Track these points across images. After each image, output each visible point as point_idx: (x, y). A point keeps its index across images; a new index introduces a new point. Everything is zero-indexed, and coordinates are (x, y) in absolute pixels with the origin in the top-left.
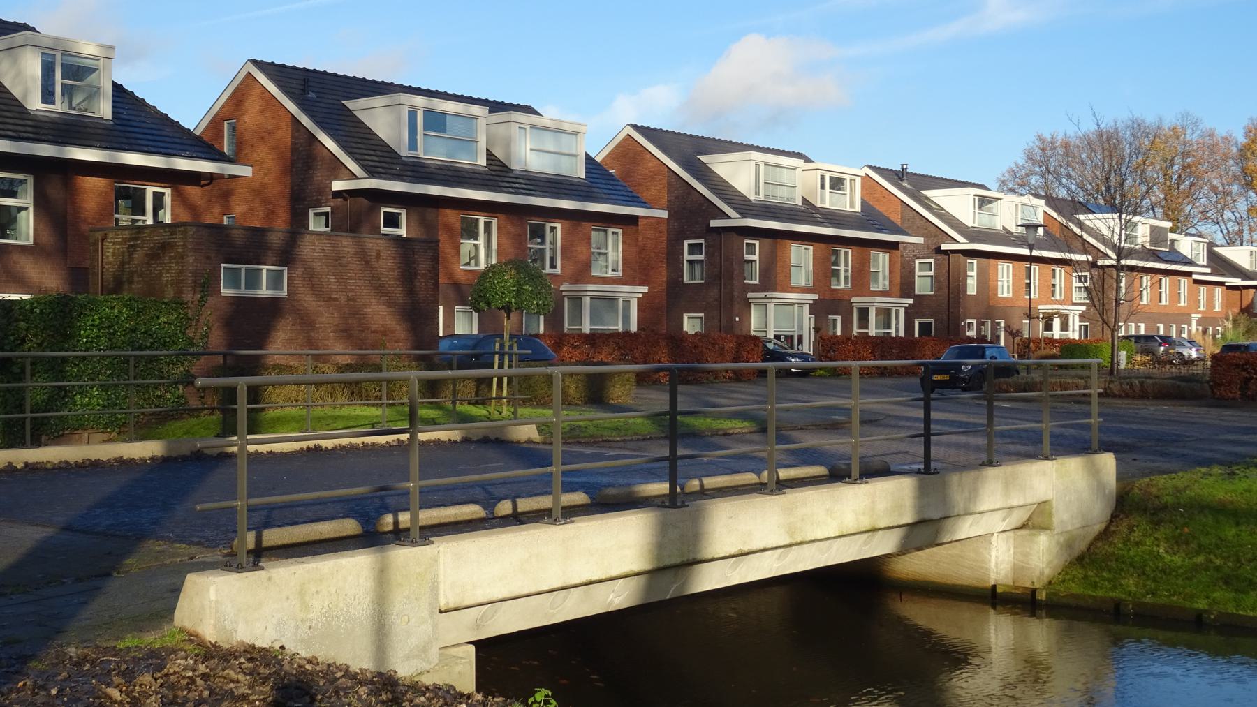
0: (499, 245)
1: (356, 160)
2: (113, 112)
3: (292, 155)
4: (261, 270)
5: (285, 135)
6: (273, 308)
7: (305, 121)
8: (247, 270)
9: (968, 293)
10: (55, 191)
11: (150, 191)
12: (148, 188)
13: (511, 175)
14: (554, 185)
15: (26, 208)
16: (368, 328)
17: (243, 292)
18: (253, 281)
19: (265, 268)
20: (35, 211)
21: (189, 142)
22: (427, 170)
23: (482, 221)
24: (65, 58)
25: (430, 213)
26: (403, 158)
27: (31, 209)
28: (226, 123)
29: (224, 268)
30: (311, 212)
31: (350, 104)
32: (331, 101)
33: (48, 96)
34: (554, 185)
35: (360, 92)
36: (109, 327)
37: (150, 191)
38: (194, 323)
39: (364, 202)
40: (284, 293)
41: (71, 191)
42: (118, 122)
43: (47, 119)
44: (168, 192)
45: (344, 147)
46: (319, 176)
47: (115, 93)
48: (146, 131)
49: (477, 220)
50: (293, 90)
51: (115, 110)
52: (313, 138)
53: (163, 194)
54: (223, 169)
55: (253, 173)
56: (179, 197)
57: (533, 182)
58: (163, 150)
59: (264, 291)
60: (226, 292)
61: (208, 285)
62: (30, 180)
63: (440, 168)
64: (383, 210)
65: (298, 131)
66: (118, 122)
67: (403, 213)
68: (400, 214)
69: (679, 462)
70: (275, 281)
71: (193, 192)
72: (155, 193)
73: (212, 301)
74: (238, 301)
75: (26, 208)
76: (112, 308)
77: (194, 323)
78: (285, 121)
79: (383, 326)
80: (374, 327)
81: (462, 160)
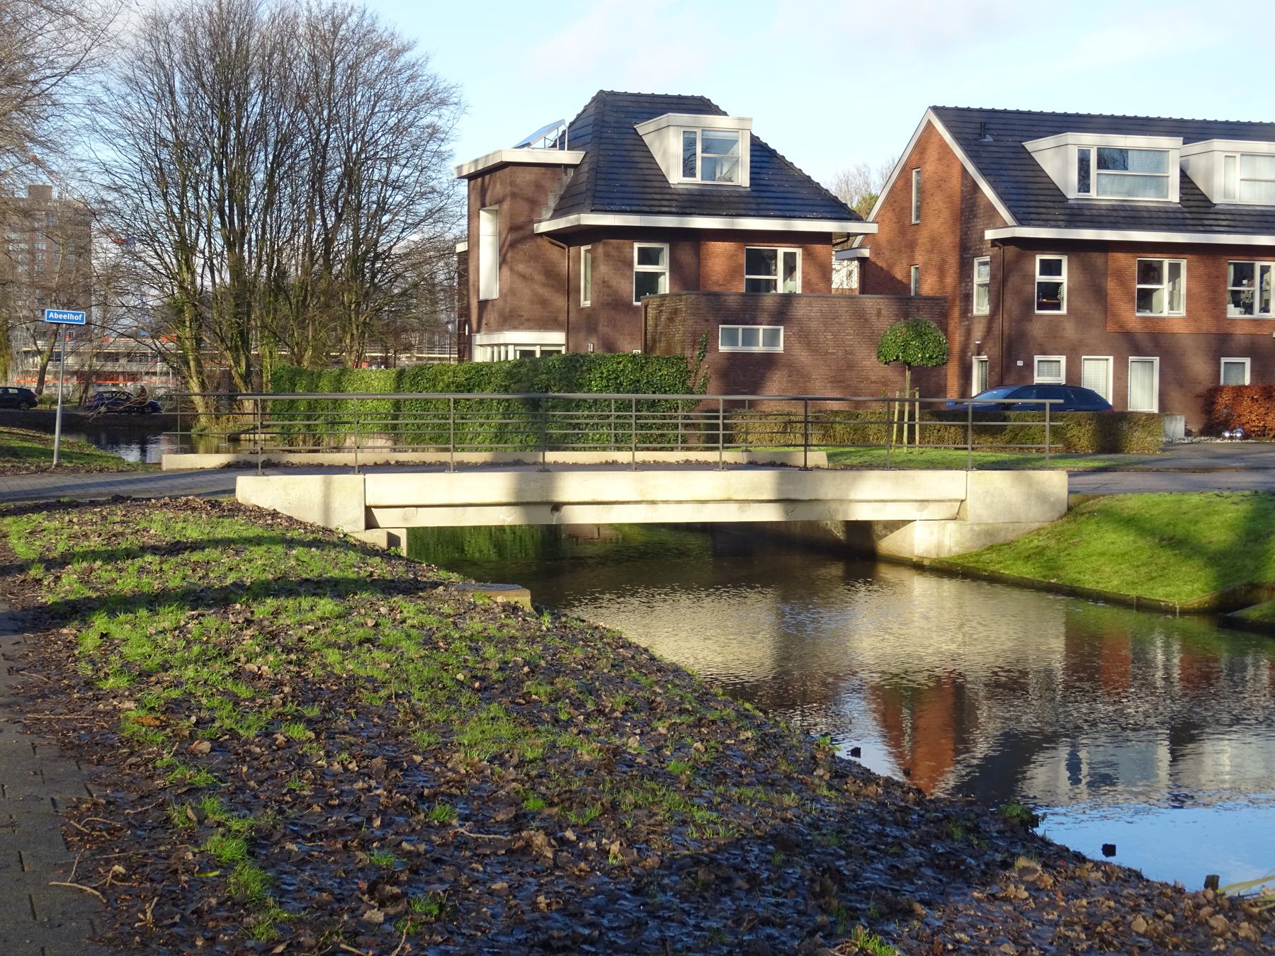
0: (1188, 290)
1: (1009, 208)
2: (751, 179)
3: (962, 204)
4: (758, 329)
5: (955, 182)
6: (768, 361)
7: (971, 169)
9: (1064, 383)
10: (686, 256)
11: (781, 251)
13: (1212, 210)
14: (1209, 228)
15: (664, 274)
16: (867, 379)
17: (740, 348)
18: (750, 338)
19: (761, 328)
20: (670, 275)
21: (821, 203)
22: (1095, 212)
23: (1166, 263)
25: (1098, 258)
26: (1070, 202)
27: (667, 274)
28: (914, 172)
30: (976, 262)
31: (1030, 145)
32: (1009, 144)
33: (689, 170)
34: (1209, 228)
35: (1026, 134)
36: (616, 378)
38: (693, 375)
39: (1012, 250)
40: (780, 349)
42: (756, 188)
43: (685, 192)
44: (799, 252)
45: (1001, 196)
46: (979, 223)
47: (754, 164)
48: (780, 195)
49: (1161, 262)
50: (966, 136)
51: (754, 176)
52: (976, 187)
53: (794, 254)
54: (843, 228)
55: (879, 229)
56: (808, 256)
57: (1229, 217)
58: (787, 214)
59: (760, 348)
60: (723, 349)
61: (705, 344)
62: (666, 248)
63: (1114, 209)
64: (1038, 258)
65: (966, 179)
66: (756, 188)
67: (1065, 260)
68: (1060, 261)
69: (489, 349)
70: (772, 338)
72: (785, 254)
73: (709, 357)
75: (664, 274)
76: (619, 363)
77: (693, 375)
78: (956, 171)
79: (883, 377)
80: (873, 378)
81: (1147, 198)
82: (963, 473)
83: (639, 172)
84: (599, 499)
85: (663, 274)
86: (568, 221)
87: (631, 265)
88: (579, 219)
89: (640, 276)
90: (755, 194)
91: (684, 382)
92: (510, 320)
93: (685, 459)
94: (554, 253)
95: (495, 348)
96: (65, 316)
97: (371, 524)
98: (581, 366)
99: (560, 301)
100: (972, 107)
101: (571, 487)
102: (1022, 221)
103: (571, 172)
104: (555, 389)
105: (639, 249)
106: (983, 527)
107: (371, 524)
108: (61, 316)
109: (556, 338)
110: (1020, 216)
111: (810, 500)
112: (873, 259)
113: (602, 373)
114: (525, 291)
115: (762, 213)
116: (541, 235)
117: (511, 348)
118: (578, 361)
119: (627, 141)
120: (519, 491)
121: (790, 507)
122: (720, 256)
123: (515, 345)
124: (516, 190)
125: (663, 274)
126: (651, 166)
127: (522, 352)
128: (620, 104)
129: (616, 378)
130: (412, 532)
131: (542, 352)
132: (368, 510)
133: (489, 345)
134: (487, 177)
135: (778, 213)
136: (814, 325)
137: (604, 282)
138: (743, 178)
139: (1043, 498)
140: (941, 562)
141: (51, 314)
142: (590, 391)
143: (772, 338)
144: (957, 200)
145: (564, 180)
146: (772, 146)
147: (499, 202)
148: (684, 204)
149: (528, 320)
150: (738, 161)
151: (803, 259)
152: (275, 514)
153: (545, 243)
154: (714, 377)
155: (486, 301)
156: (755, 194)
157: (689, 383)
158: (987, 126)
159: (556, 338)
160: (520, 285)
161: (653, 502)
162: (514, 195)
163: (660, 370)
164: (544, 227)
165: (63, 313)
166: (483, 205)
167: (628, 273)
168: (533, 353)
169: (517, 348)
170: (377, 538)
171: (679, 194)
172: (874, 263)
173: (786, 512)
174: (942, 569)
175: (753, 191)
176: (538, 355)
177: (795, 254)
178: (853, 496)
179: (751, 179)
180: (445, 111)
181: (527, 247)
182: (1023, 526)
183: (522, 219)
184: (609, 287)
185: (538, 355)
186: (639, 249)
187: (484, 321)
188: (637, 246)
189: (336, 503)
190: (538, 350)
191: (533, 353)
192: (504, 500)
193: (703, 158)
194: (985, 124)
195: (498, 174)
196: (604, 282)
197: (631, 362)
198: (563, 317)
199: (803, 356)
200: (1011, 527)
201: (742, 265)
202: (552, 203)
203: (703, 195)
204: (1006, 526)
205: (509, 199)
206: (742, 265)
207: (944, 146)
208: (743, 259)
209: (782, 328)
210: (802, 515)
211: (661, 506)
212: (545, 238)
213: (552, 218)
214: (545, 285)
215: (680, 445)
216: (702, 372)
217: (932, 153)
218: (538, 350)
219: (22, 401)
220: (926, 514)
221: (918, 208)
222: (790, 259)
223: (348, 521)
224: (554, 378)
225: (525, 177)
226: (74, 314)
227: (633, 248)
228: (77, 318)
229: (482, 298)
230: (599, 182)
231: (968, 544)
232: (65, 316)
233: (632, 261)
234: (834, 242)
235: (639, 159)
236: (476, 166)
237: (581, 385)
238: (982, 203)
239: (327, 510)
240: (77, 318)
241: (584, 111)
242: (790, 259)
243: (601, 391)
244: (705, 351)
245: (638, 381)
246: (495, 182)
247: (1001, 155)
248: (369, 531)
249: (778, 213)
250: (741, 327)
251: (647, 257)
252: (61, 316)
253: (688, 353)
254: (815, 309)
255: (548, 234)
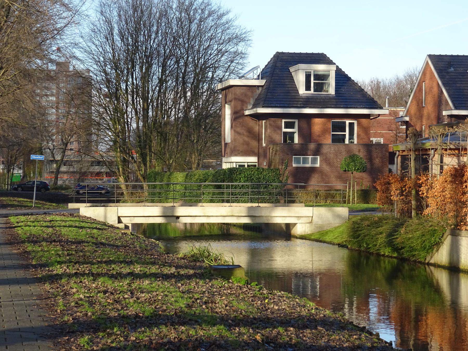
1: (453, 102)
6: (312, 170)
8: (303, 158)
11: (348, 122)
12: (346, 121)
17: (301, 165)
18: (305, 161)
20: (298, 133)
24: (315, 72)
27: (297, 132)
29: (294, 158)
33: (308, 88)
36: (251, 177)
37: (348, 122)
40: (318, 165)
41: (310, 126)
43: (306, 97)
44: (355, 122)
45: (450, 96)
59: (309, 165)
60: (294, 165)
69: (230, 164)
71: (364, 121)
72: (350, 123)
73: (289, 169)
74: (297, 168)
79: (361, 176)
80: (357, 177)
82: (312, 208)
83: (287, 89)
84: (190, 215)
85: (296, 132)
86: (253, 111)
87: (281, 129)
88: (256, 110)
89: (285, 133)
90: (337, 98)
91: (278, 178)
92: (235, 152)
93: (251, 206)
94: (252, 123)
95: (232, 163)
96: (37, 157)
97: (120, 221)
98: (236, 172)
99: (254, 143)
100: (447, 54)
101: (181, 211)
102: (456, 108)
103: (260, 89)
104: (226, 181)
105: (285, 122)
106: (318, 225)
107: (120, 221)
108: (36, 157)
109: (253, 160)
110: (456, 105)
111: (259, 216)
112: (410, 122)
113: (245, 175)
114: (240, 139)
115: (337, 106)
116: (247, 115)
117: (234, 164)
118: (235, 171)
119: (284, 75)
120: (164, 212)
121: (253, 218)
122: (318, 124)
123: (236, 162)
124: (237, 97)
125: (296, 132)
126: (293, 86)
127: (239, 165)
128: (285, 58)
129: (251, 177)
130: (133, 225)
131: (248, 166)
132: (119, 218)
133: (230, 162)
134: (227, 90)
135: (345, 106)
136: (332, 156)
137: (269, 136)
138: (332, 91)
139: (339, 216)
140: (301, 235)
141: (33, 157)
142: (240, 182)
143: (314, 161)
144: (436, 96)
145: (257, 92)
146: (349, 76)
147: (231, 101)
148: (304, 103)
149: (242, 152)
150: (330, 84)
151: (357, 125)
152: (95, 220)
153: (248, 119)
154: (291, 176)
155: (227, 143)
156: (337, 98)
157: (281, 179)
158: (452, 63)
159: (253, 160)
160: (238, 137)
161: (208, 216)
162: (235, 99)
163: (269, 174)
164: (247, 113)
165: (37, 156)
166: (226, 103)
167: (279, 132)
168: (244, 166)
169: (237, 164)
170: (121, 226)
171: (303, 99)
172: (410, 123)
173: (252, 220)
174: (303, 237)
175: (336, 96)
176: (246, 166)
177: (354, 123)
178: (273, 215)
179: (336, 91)
180: (242, 44)
181: (241, 120)
182: (333, 225)
183: (239, 108)
184: (271, 138)
185: (246, 166)
186: (285, 122)
187: (226, 152)
188: (283, 121)
189: (108, 215)
190: (246, 164)
191: (244, 166)
192: (160, 215)
193: (314, 83)
194: (450, 62)
195: (230, 89)
196: (269, 136)
197: (257, 171)
198: (256, 151)
199: (326, 168)
200: (328, 225)
201: (330, 128)
202: (252, 101)
203: (313, 99)
204: (327, 225)
205: (233, 100)
206: (330, 128)
207: (432, 73)
208: (330, 126)
209: (319, 157)
210: (258, 221)
211: (211, 217)
212: (249, 117)
213: (252, 108)
214: (248, 137)
215: (315, 204)
216: (286, 174)
217: (428, 76)
218: (246, 164)
219: (42, 188)
220: (300, 221)
221: (425, 100)
222: (351, 125)
223: (112, 221)
224: (226, 177)
225: (238, 91)
226: (40, 157)
227: (282, 122)
228: (41, 158)
229: (226, 142)
230: (269, 94)
231: (313, 231)
232: (37, 157)
233: (282, 127)
234: (371, 118)
235: (287, 83)
236: (222, 86)
237: (237, 180)
238: (444, 99)
239: (105, 217)
240: (41, 158)
241: (271, 60)
242: (351, 125)
243: (245, 182)
244: (287, 166)
245: (260, 178)
246: (229, 93)
247: (455, 77)
248: (119, 224)
249: (345, 106)
250: (302, 157)
251: (288, 125)
252: (36, 157)
253: (280, 167)
254: (332, 149)
255: (250, 115)
